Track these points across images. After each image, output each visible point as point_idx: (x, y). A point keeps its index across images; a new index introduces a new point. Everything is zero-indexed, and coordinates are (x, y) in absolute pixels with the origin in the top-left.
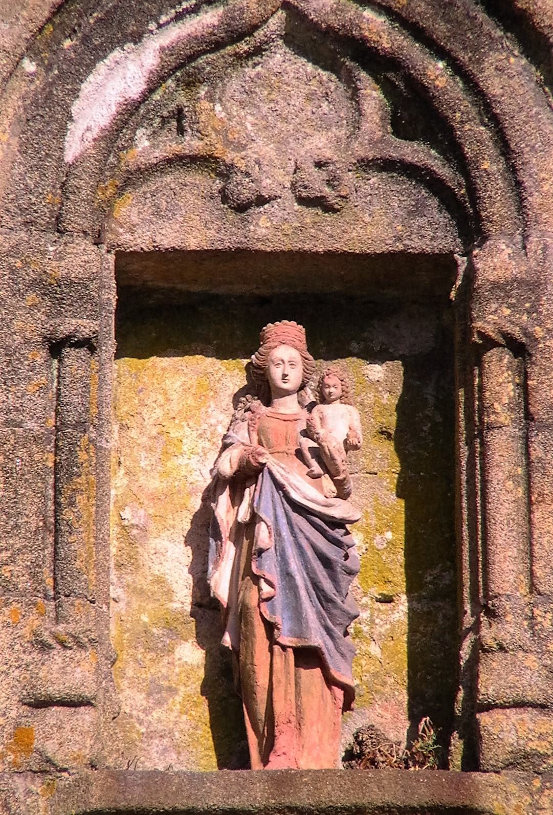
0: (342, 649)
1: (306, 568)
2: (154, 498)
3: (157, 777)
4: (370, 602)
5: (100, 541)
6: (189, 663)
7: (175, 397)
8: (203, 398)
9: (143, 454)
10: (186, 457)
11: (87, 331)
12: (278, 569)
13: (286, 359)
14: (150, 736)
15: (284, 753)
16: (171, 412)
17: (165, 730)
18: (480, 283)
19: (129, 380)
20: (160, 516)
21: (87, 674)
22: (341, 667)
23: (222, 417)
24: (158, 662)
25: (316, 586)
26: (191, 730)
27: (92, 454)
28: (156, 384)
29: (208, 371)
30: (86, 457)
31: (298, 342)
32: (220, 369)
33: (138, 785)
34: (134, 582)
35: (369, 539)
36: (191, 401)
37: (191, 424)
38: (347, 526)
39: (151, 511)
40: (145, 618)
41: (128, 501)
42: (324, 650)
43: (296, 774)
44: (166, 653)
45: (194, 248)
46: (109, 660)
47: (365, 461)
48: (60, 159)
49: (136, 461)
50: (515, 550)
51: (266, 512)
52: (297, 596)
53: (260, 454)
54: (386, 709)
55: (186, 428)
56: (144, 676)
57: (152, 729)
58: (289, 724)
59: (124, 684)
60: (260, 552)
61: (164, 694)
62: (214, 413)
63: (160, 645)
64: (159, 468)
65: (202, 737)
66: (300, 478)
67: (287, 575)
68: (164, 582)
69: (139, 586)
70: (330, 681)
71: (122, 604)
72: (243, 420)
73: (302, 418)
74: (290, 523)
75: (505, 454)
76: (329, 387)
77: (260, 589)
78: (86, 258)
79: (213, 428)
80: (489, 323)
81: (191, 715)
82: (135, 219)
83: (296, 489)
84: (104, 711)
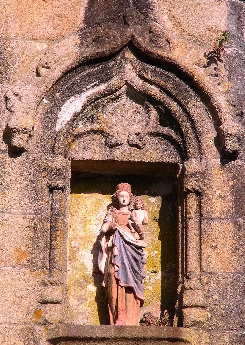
2: (81, 238)
4: (149, 273)
5: (64, 252)
7: (89, 206)
9: (78, 224)
10: (92, 225)
11: (61, 185)
12: (120, 262)
19: (74, 201)
20: (83, 244)
21: (59, 294)
24: (82, 291)
25: (133, 268)
27: (62, 224)
29: (100, 198)
33: (74, 329)
35: (149, 253)
36: (94, 208)
37: (94, 215)
39: (80, 243)
40: (78, 276)
42: (134, 288)
45: (96, 159)
48: (54, 130)
50: (196, 257)
53: (116, 225)
54: (154, 307)
56: (77, 295)
57: (79, 311)
60: (115, 256)
61: (83, 301)
62: (101, 212)
66: (128, 233)
67: (123, 264)
69: (76, 266)
70: (136, 298)
71: (70, 272)
72: (110, 214)
74: (124, 247)
75: (193, 227)
76: (138, 204)
77: (114, 268)
79: (100, 216)
80: (189, 185)
82: (77, 150)
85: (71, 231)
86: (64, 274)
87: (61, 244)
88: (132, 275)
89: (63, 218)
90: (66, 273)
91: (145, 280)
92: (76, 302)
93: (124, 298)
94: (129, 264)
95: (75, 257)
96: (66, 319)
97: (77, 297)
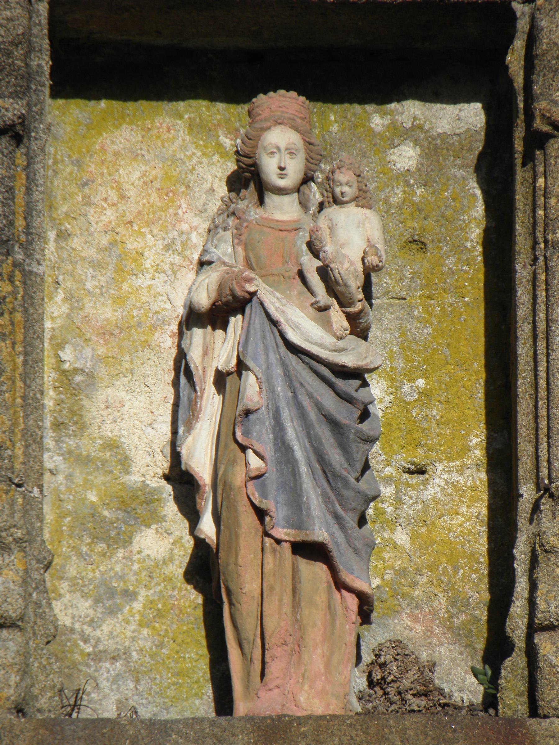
0: (356, 543)
1: (308, 435)
2: (105, 332)
3: (105, 728)
4: (394, 473)
5: (30, 401)
6: (153, 558)
7: (132, 193)
8: (171, 194)
10: (148, 276)
11: (10, 115)
12: (271, 436)
13: (283, 146)
14: (98, 657)
15: (278, 687)
16: (128, 213)
17: (119, 650)
18: (544, 47)
19: (68, 169)
20: (113, 357)
21: (12, 586)
22: (355, 568)
23: (196, 221)
24: (110, 557)
25: (321, 458)
26: (154, 649)
28: (106, 175)
29: (178, 156)
30: (9, 288)
31: (299, 120)
32: (194, 154)
33: (79, 738)
34: (78, 447)
35: (394, 386)
36: (154, 198)
37: (155, 231)
38: (367, 375)
39: (101, 351)
40: (93, 497)
41: (69, 337)
42: (331, 546)
43: (290, 722)
44: (121, 544)
46: (42, 563)
47: (389, 281)
49: (80, 282)
51: (255, 359)
52: (295, 473)
56: (90, 575)
57: (101, 648)
58: (285, 647)
59: (64, 587)
61: (118, 600)
62: (186, 216)
63: (113, 534)
64: (112, 292)
65: (168, 658)
66: (299, 312)
69: (84, 453)
70: (340, 585)
71: (60, 478)
72: (225, 229)
73: (305, 226)
74: (287, 375)
76: (341, 184)
77: (247, 464)
78: (8, 13)
79: (184, 236)
81: (154, 628)
83: (297, 327)
84: (34, 633)
85: (60, 302)
86: (35, 497)
87: (14, 370)
88: (319, 490)
89: (20, 257)
90: (41, 491)
91: (380, 505)
92: (85, 606)
93: (289, 589)
94: (307, 444)
95: (81, 416)
96: (43, 690)
97: (91, 587)
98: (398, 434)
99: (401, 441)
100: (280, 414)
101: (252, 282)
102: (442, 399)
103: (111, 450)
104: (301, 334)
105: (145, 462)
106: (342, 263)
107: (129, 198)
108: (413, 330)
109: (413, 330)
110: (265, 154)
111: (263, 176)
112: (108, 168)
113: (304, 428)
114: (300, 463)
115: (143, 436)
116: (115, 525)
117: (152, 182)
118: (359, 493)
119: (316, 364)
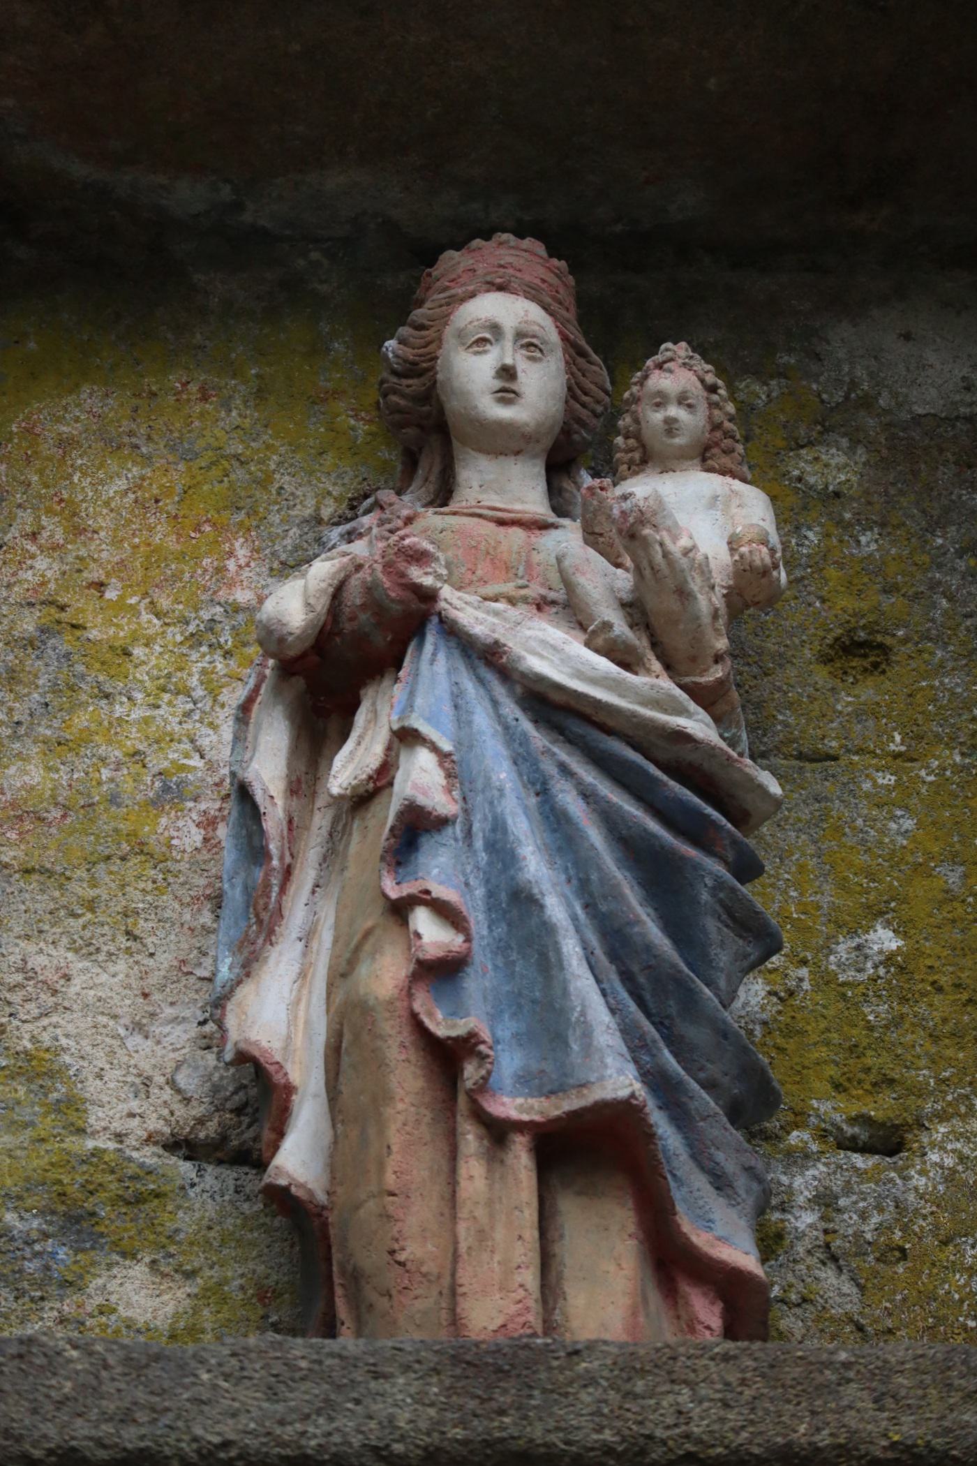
0: (720, 1156)
22: (716, 1216)
25: (616, 943)
32: (268, 447)
36: (163, 535)
52: (546, 961)
55: (146, 617)
62: (246, 573)
67: (518, 904)
68: (51, 1074)
79: (241, 617)
98: (823, 1052)
99: (831, 1071)
100: (505, 831)
101: (427, 564)
102: (944, 980)
103: (30, 1080)
104: (562, 660)
105: (124, 1108)
106: (675, 539)
107: (95, 532)
108: (860, 822)
109: (860, 822)
110: (460, 349)
111: (453, 405)
112: (41, 472)
113: (572, 872)
114: (562, 932)
115: (120, 1052)
116: (37, 1247)
117: (157, 501)
118: (725, 1036)
119: (602, 736)
